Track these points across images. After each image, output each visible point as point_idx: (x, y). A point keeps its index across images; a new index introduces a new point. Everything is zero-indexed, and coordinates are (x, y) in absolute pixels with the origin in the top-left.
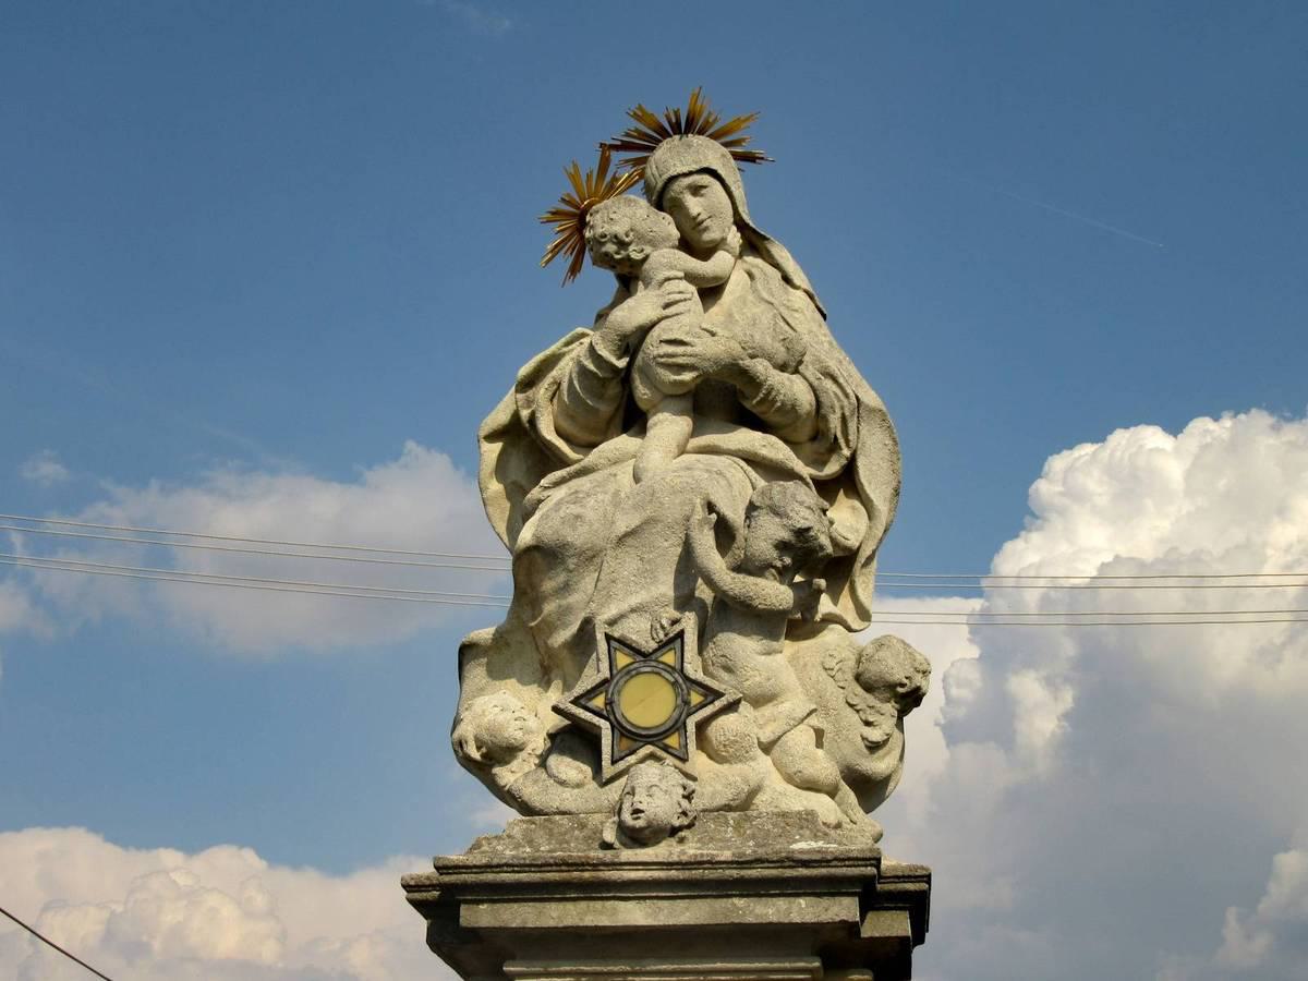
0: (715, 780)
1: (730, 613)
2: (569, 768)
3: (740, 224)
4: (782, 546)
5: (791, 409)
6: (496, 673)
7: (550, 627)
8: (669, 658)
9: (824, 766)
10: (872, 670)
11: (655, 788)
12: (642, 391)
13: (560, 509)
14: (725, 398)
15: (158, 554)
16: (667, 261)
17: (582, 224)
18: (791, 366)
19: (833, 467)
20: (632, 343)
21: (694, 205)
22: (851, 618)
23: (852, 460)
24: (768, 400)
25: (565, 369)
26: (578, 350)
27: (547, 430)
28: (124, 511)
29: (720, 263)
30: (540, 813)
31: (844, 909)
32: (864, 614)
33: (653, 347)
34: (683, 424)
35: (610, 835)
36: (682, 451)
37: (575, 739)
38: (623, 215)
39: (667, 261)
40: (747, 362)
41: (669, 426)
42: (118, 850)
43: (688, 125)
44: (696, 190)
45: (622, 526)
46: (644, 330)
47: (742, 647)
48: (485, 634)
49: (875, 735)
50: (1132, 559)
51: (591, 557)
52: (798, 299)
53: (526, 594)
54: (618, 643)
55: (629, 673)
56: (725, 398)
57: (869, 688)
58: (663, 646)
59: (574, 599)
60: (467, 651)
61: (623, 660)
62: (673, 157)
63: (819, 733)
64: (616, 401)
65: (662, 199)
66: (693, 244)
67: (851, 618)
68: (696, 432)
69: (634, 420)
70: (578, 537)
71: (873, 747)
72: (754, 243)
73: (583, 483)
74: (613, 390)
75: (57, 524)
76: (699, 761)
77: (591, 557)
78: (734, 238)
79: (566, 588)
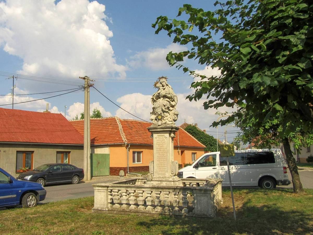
0: (164, 122)
1: (164, 112)
2: (156, 121)
3: (166, 84)
4: (167, 108)
5: (169, 97)
6: (152, 114)
7: (155, 112)
8: (161, 115)
9: (171, 120)
10: (175, 113)
11: (160, 123)
12: (160, 97)
13: (156, 104)
14: (165, 97)
15: (143, 60)
16: (161, 88)
17: (156, 85)
18: (169, 94)
19: (173, 100)
20: (159, 94)
21: (163, 84)
22: (174, 109)
23: (174, 99)
24: (168, 97)
25: (155, 95)
26: (156, 94)
27: (155, 99)
28: (138, 55)
29: (165, 87)
30: (45, 204)
31: (170, 129)
32: (175, 109)
33: (160, 94)
34: (163, 98)
35: (157, 126)
36: (163, 100)
37: (156, 119)
38: (158, 85)
39: (161, 88)
40: (166, 95)
41: (162, 99)
42: (144, 95)
43: (163, 78)
44: (163, 83)
45: (158, 106)
46: (160, 93)
47: (165, 113)
48: (151, 112)
49: (175, 117)
50: (46, 194)
51: (157, 108)
52: (170, 88)
53: (153, 110)
54: (158, 114)
55: (159, 116)
56: (165, 97)
57: (175, 114)
58: (160, 114)
59: (156, 110)
60: (151, 113)
61: (158, 115)
62: (161, 80)
63: (170, 118)
64: (158, 97)
65: (161, 83)
66: (163, 86)
67: (174, 109)
68: (163, 99)
69: (160, 98)
70: (156, 107)
71: (175, 118)
72: (167, 85)
73: (156, 103)
74: (158, 96)
75: (131, 57)
76: (163, 120)
77: (157, 108)
78: (166, 85)
79: (155, 110)
